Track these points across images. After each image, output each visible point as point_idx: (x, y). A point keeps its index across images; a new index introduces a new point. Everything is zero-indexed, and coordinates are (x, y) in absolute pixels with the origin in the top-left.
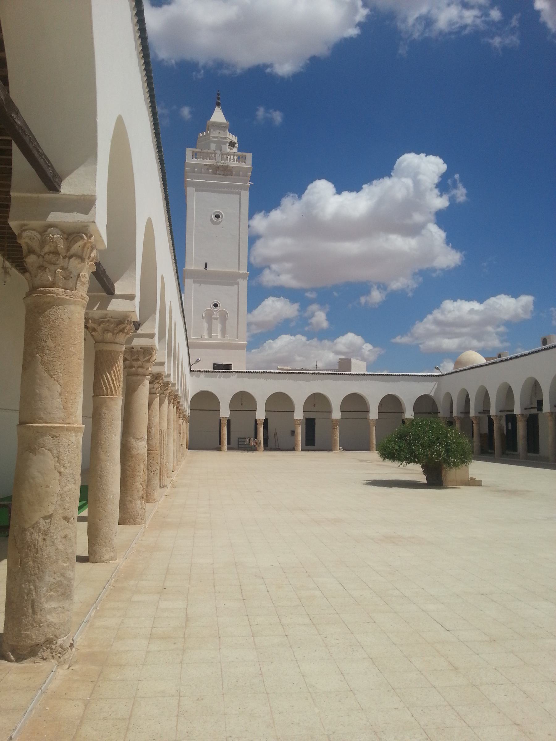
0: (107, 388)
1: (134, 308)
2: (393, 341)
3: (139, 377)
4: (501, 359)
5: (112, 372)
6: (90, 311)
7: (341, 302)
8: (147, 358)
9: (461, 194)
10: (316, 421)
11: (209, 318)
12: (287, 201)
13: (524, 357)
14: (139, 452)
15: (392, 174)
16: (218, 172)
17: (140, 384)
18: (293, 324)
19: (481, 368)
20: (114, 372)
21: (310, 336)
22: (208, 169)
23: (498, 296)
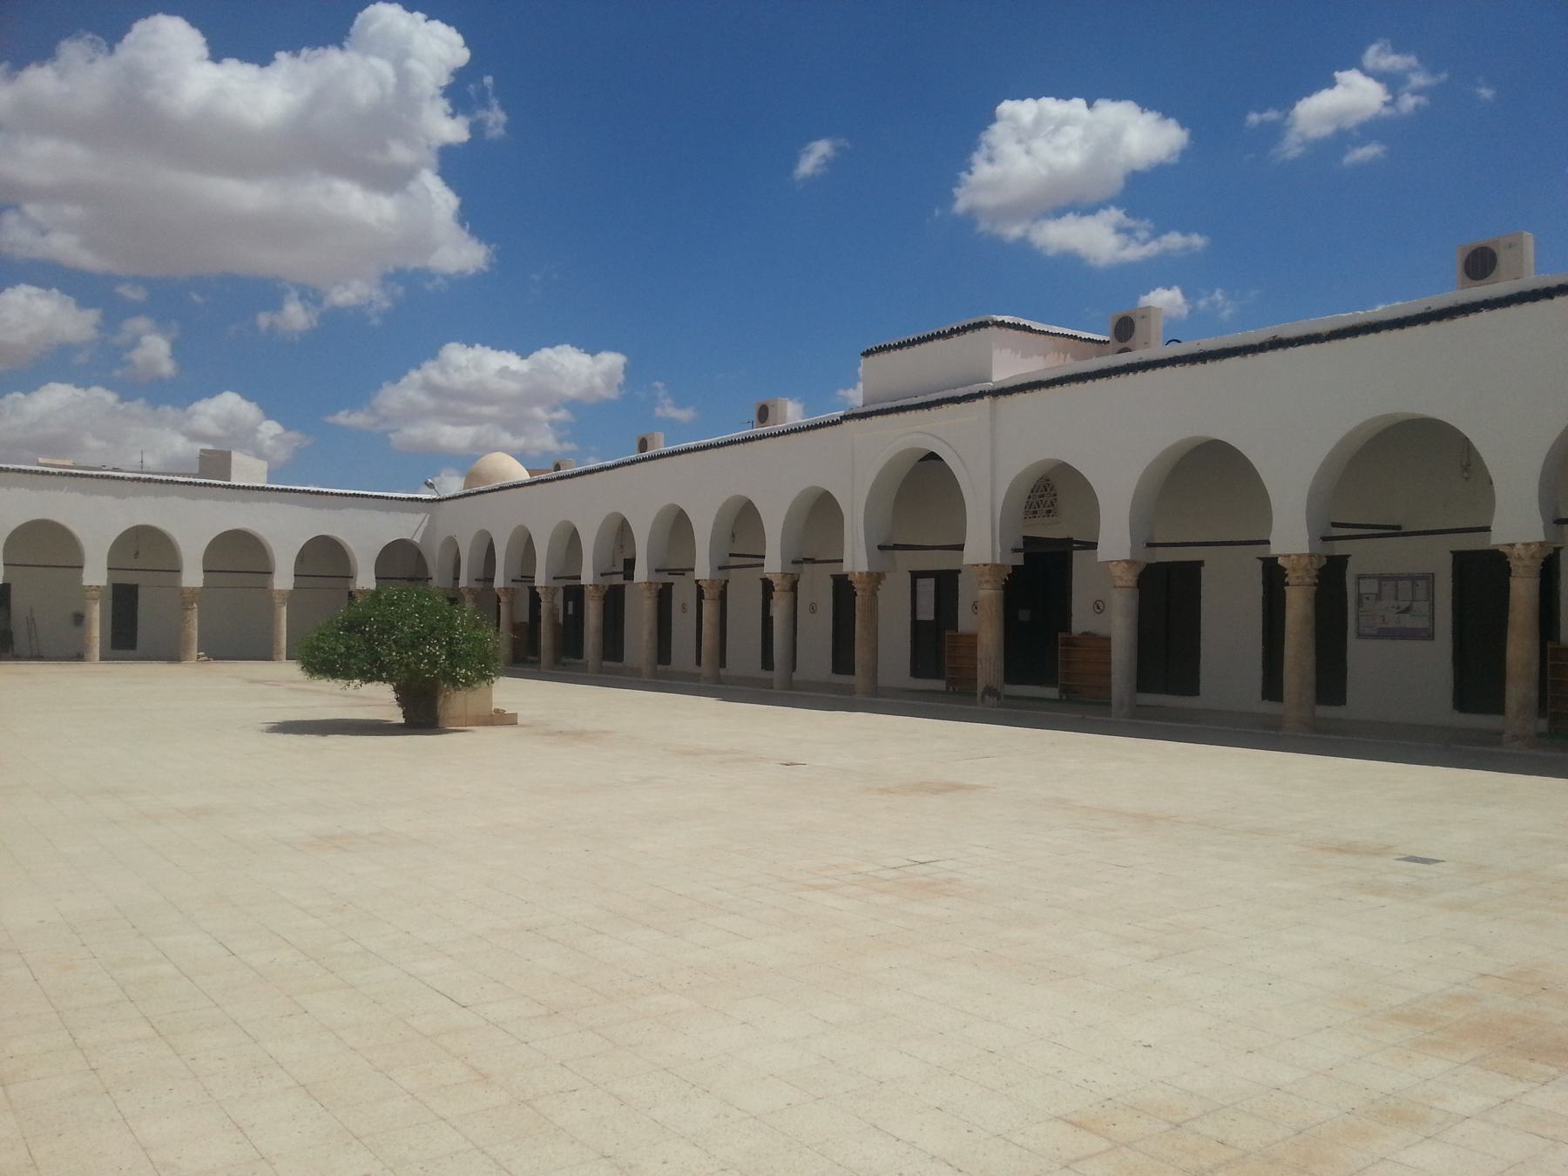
2: (330, 419)
4: (562, 472)
9: (496, 118)
10: (141, 591)
12: (72, 50)
15: (345, 44)
23: (558, 348)
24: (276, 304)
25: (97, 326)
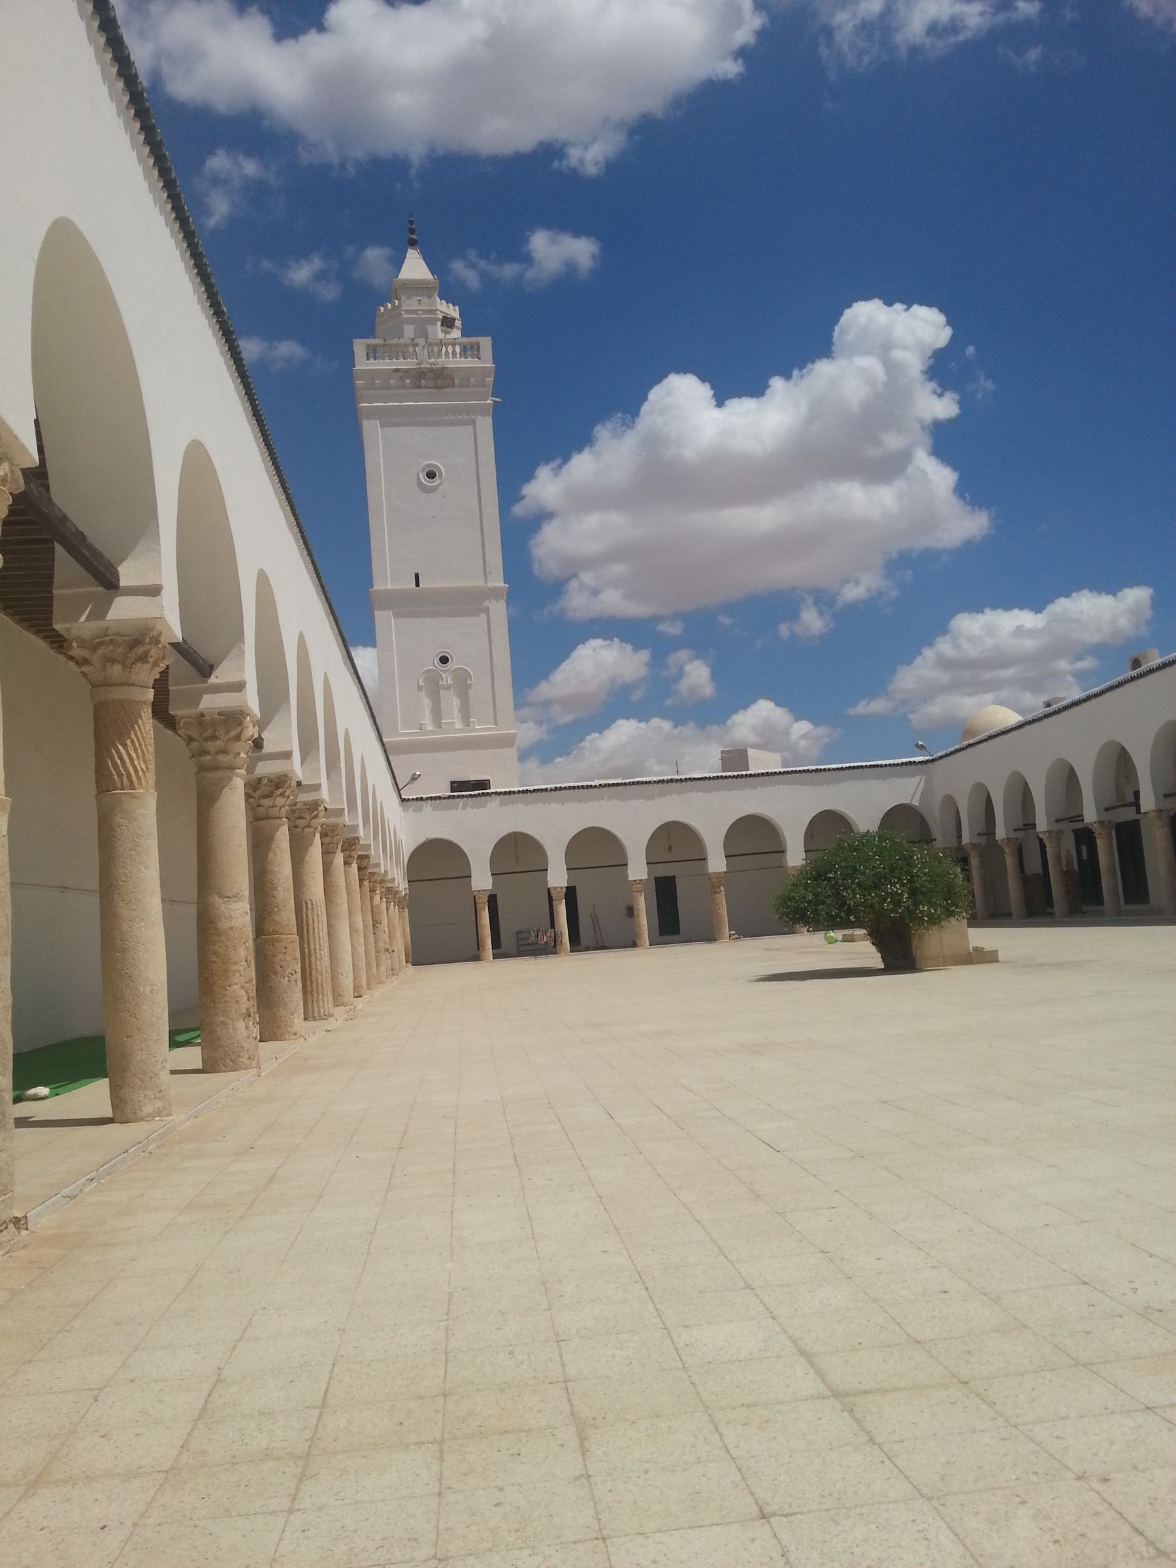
0: (120, 776)
1: (168, 615)
2: (852, 711)
3: (221, 773)
5: (128, 742)
6: (73, 625)
7: (740, 637)
8: (233, 733)
11: (433, 686)
12: (602, 432)
13: (1093, 701)
14: (233, 923)
16: (423, 382)
17: (224, 787)
18: (636, 696)
19: (1010, 735)
20: (132, 742)
21: (679, 717)
22: (402, 379)
24: (793, 614)
25: (648, 664)
